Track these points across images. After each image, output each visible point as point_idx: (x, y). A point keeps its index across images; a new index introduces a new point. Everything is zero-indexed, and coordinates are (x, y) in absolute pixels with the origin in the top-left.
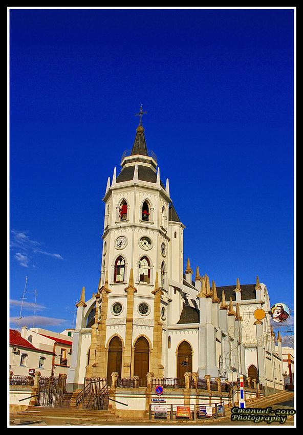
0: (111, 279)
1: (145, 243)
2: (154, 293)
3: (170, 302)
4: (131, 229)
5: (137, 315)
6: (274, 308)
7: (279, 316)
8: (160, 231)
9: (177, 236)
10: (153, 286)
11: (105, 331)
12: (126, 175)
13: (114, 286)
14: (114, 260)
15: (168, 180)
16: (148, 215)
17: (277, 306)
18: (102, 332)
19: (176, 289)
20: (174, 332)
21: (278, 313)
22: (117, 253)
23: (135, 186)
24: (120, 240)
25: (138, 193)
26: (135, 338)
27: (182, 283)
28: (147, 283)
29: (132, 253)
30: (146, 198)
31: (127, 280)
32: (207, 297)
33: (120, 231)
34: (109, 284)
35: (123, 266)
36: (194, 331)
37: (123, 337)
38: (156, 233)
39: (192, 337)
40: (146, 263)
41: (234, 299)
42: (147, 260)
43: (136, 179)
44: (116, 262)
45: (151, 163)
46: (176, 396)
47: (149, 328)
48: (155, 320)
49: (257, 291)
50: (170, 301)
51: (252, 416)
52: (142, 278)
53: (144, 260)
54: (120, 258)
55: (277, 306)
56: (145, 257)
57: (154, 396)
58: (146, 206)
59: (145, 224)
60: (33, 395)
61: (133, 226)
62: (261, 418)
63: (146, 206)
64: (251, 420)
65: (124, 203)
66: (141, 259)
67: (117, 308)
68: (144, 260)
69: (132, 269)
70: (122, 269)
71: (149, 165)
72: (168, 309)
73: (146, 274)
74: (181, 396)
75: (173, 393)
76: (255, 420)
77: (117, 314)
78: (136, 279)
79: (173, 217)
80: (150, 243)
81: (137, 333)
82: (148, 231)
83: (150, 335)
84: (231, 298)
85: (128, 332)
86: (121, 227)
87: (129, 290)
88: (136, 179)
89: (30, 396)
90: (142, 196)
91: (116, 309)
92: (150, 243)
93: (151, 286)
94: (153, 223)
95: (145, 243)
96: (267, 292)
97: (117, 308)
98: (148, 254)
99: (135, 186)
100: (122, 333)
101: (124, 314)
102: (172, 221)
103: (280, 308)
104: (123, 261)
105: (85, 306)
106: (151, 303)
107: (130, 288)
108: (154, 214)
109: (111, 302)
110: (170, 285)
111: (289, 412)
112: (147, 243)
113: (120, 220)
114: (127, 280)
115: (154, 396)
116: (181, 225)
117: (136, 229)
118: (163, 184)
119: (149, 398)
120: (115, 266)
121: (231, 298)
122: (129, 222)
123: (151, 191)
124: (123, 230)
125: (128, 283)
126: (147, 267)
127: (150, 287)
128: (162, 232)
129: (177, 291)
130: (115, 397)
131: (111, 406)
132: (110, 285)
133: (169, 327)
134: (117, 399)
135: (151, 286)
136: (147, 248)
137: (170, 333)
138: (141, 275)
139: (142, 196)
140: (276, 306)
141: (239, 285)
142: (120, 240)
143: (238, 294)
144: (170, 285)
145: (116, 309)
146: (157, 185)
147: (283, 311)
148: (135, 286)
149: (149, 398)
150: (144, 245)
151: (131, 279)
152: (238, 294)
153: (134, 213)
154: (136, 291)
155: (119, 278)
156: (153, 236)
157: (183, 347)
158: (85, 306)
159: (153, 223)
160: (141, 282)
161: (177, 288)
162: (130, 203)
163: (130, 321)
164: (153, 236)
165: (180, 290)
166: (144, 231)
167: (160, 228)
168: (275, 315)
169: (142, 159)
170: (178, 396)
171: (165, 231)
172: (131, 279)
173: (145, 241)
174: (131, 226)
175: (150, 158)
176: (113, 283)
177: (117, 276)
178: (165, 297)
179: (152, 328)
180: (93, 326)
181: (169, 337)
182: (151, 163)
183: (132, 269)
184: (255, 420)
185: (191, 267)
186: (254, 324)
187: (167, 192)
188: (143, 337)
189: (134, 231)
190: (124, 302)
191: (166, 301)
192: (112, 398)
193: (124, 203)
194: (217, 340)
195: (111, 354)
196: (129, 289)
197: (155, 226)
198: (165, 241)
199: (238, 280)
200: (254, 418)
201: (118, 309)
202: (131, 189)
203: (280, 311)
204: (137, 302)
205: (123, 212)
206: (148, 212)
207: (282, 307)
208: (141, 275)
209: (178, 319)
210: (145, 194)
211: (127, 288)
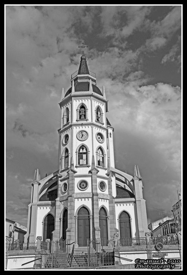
0: (75, 162)
1: (99, 138)
2: (90, 172)
22: (80, 143)
29: (92, 144)
33: (81, 127)
39: (130, 209)
40: (101, 153)
43: (91, 92)
44: (79, 150)
46: (173, 251)
51: (149, 265)
54: (83, 147)
57: (154, 252)
60: (37, 258)
62: (156, 266)
64: (149, 267)
65: (83, 107)
69: (93, 156)
70: (84, 156)
74: (177, 251)
75: (170, 248)
76: (152, 267)
87: (93, 172)
88: (91, 92)
89: (34, 259)
91: (81, 185)
97: (83, 185)
100: (88, 204)
105: (39, 184)
106: (88, 180)
109: (77, 181)
111: (156, 261)
112: (100, 138)
114: (90, 163)
115: (154, 252)
119: (150, 253)
120: (79, 153)
122: (88, 121)
130: (119, 254)
131: (117, 262)
134: (121, 256)
138: (98, 161)
148: (75, 169)
149: (150, 253)
153: (91, 116)
155: (83, 162)
157: (123, 216)
170: (175, 251)
172: (93, 163)
173: (99, 136)
176: (78, 165)
177: (80, 160)
180: (56, 199)
183: (93, 156)
184: (152, 267)
192: (118, 255)
193: (83, 107)
195: (80, 221)
196: (93, 170)
197: (90, 121)
200: (151, 266)
208: (98, 161)
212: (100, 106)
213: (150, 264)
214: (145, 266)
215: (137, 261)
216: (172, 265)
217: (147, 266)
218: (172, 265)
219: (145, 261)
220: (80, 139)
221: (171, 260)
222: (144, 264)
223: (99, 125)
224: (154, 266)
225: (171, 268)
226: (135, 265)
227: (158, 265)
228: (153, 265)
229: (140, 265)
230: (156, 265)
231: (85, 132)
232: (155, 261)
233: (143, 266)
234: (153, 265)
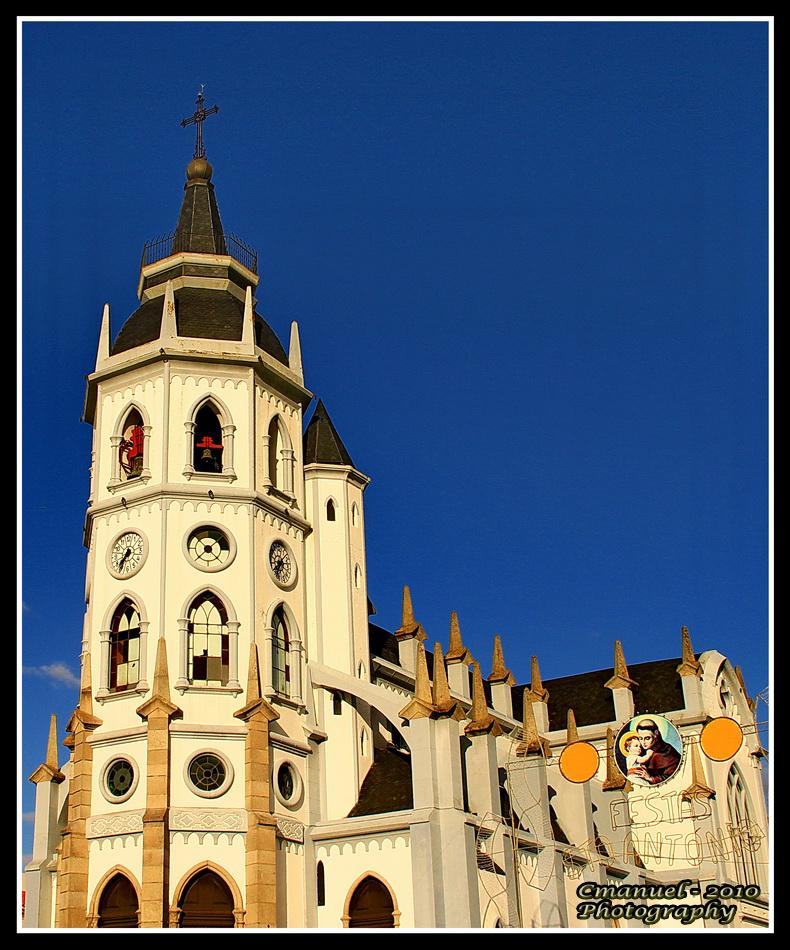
1: (208, 549)
2: (243, 715)
3: (319, 742)
4: (155, 506)
5: (184, 795)
6: (626, 736)
7: (646, 763)
8: (259, 502)
9: (339, 512)
10: (241, 691)
11: (86, 858)
12: (138, 327)
13: (110, 705)
14: (111, 606)
15: (295, 325)
16: (218, 453)
17: (639, 727)
18: (74, 865)
19: (339, 696)
20: (334, 848)
21: (643, 753)
23: (164, 357)
24: (124, 546)
25: (177, 381)
26: (180, 872)
27: (366, 675)
28: (217, 684)
30: (126, 402)
31: (149, 680)
32: (435, 716)
33: (123, 515)
34: (94, 695)
35: (135, 633)
36: (400, 841)
37: (136, 873)
38: (245, 510)
41: (611, 716)
42: (218, 604)
43: (169, 339)
44: (115, 621)
45: (232, 274)
47: (217, 838)
48: (252, 808)
49: (688, 681)
50: (318, 739)
52: (201, 667)
53: (207, 605)
54: (125, 607)
55: (639, 727)
56: (206, 596)
58: (207, 423)
59: (206, 483)
61: (163, 493)
63: (207, 423)
65: (134, 418)
66: (196, 603)
67: (120, 777)
68: (207, 605)
69: (162, 642)
71: (223, 284)
72: (314, 769)
73: (216, 651)
76: (646, 915)
77: (213, 793)
78: (177, 671)
79: (319, 449)
80: (224, 545)
81: (185, 860)
82: (216, 507)
83: (235, 863)
84: (571, 715)
85: (150, 856)
86: (124, 502)
88: (169, 339)
90: (188, 390)
91: (117, 779)
92: (224, 545)
93: (232, 691)
94: (235, 478)
95: (208, 549)
96: (736, 681)
97: (120, 777)
98: (218, 583)
99: (164, 357)
101: (139, 799)
102: (313, 465)
103: (648, 733)
104: (135, 615)
105: (58, 779)
106: (234, 755)
107: (157, 704)
108: (240, 450)
110: (314, 686)
112: (216, 547)
113: (124, 476)
116: (351, 476)
117: (175, 505)
118: (266, 337)
121: (571, 715)
123: (222, 370)
124: (134, 512)
125: (151, 687)
126: (218, 630)
127: (229, 698)
128: (274, 505)
129: (343, 702)
132: (98, 699)
133: (316, 832)
135: (232, 691)
136: (215, 565)
137: (321, 853)
139: (188, 390)
140: (633, 727)
141: (621, 665)
142: (124, 546)
143: (623, 699)
144: (314, 686)
145: (117, 779)
146: (246, 347)
147: (659, 744)
148: (177, 699)
150: (207, 556)
151: (162, 676)
152: (623, 699)
154: (178, 714)
155: (124, 674)
156: (236, 521)
158: (58, 779)
159: (235, 478)
160: (198, 683)
161: (342, 692)
162: (152, 418)
163: (160, 819)
164: (236, 521)
165: (354, 701)
166: (203, 506)
167: (263, 493)
168: (632, 758)
169: (196, 266)
171: (287, 499)
172: (162, 676)
173: (209, 541)
174: (156, 494)
175: (226, 261)
176: (106, 693)
178: (294, 727)
179: (239, 839)
181: (321, 866)
182: (232, 274)
183: (162, 642)
184: (646, 915)
185: (416, 615)
186: (684, 799)
187: (294, 369)
188: (207, 870)
189: (165, 510)
190: (136, 753)
191: (302, 740)
193: (134, 418)
194: (485, 863)
196: (153, 707)
198: (291, 537)
199: (619, 647)
200: (641, 912)
201: (122, 779)
202: (155, 369)
203: (648, 743)
204: (185, 750)
205: (133, 455)
206: (219, 441)
207: (654, 728)
209: (352, 800)
210: (204, 382)
211: (146, 707)
212: (281, 413)
213: (638, 902)
214: (617, 912)
215: (583, 893)
216: (724, 909)
217: (625, 911)
218: (724, 909)
219: (616, 892)
220: (119, 575)
221: (720, 889)
222: (615, 902)
223: (280, 507)
224: (653, 912)
225: (724, 921)
226: (578, 908)
227: (669, 907)
228: (648, 909)
229: (597, 905)
230: (662, 907)
231: (133, 533)
232: (656, 891)
233: (610, 912)
234: (648, 909)
